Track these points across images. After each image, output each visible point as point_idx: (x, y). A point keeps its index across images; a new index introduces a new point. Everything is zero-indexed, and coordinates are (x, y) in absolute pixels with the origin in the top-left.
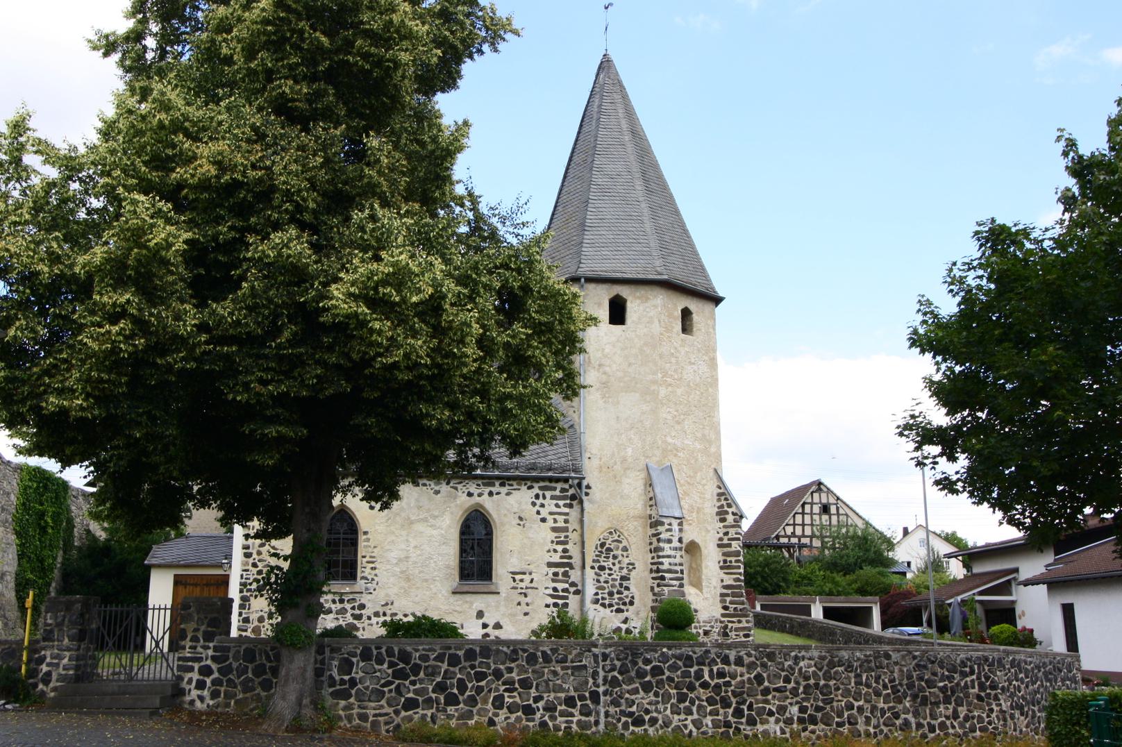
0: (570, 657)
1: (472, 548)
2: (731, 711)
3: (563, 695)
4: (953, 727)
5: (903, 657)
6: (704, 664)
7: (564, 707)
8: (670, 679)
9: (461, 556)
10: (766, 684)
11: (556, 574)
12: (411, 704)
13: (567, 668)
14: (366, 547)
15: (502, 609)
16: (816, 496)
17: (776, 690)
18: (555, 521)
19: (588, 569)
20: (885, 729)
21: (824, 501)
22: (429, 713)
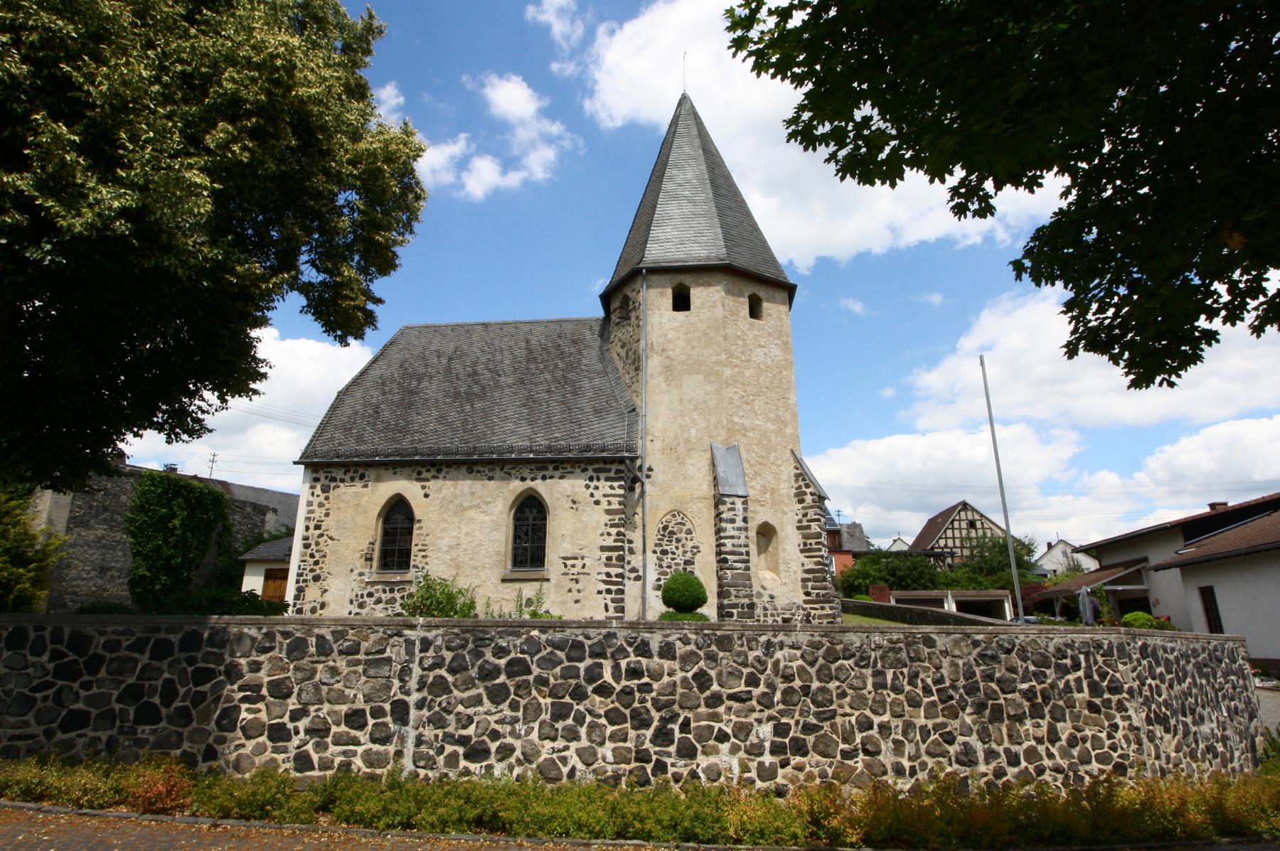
0: (364, 645)
1: (527, 534)
2: (649, 733)
3: (344, 708)
4: (1050, 756)
5: (956, 643)
6: (602, 655)
7: (343, 728)
8: (541, 681)
9: (515, 542)
10: (715, 687)
11: (609, 559)
13: (358, 663)
16: (963, 514)
17: (732, 697)
18: (609, 503)
19: (649, 553)
20: (930, 762)
21: (970, 517)
22: (104, 735)
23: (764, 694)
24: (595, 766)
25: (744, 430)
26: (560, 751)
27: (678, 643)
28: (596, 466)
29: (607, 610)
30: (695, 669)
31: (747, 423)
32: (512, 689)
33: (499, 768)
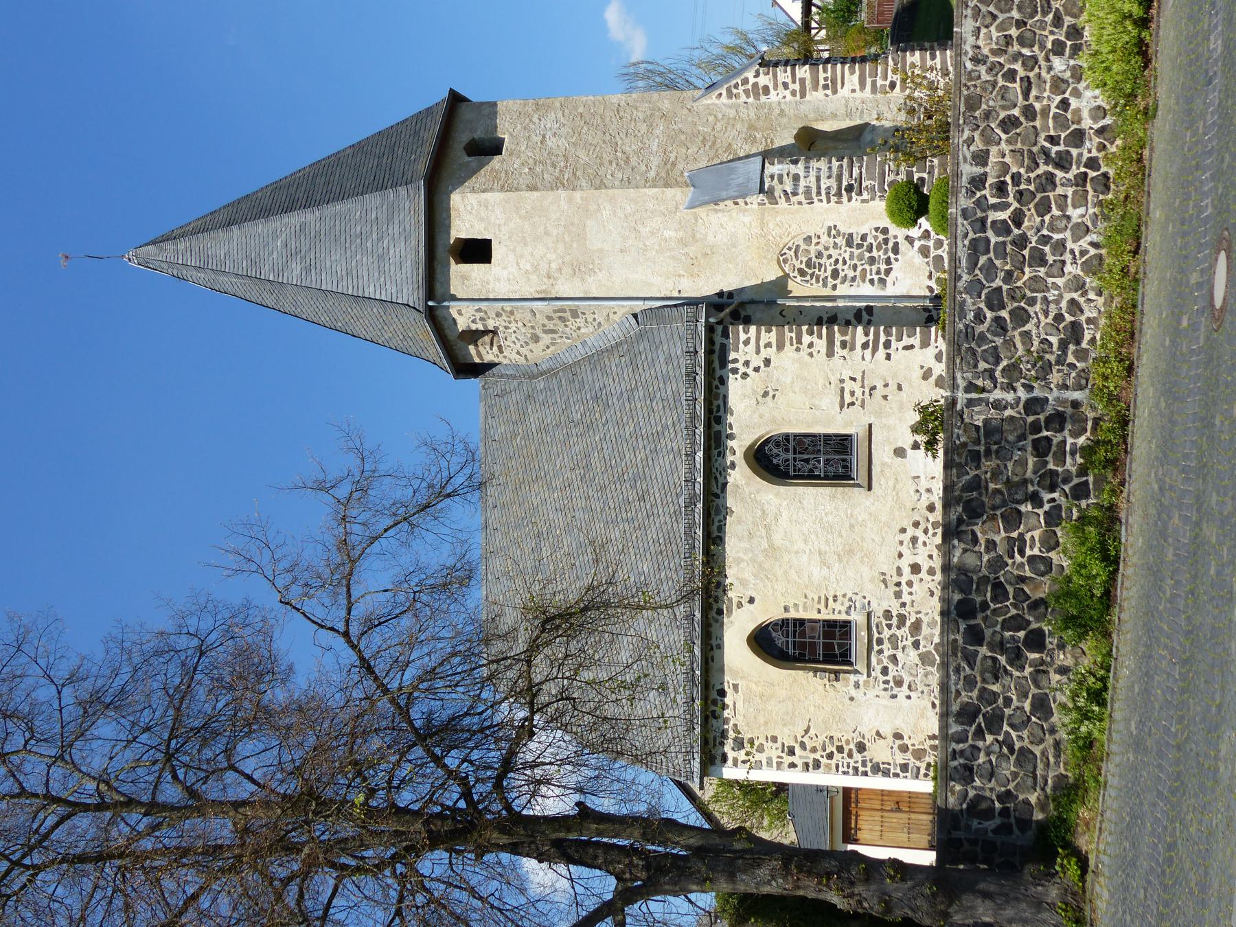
1: (807, 461)
2: (1059, 174)
6: (983, 221)
7: (1050, 458)
10: (1016, 112)
11: (844, 345)
12: (1042, 706)
14: (805, 609)
15: (892, 421)
17: (1026, 95)
18: (768, 345)
19: (837, 293)
23: (1023, 64)
24: (1089, 224)
25: (669, 163)
26: (1074, 257)
27: (972, 148)
28: (716, 364)
29: (912, 347)
30: (998, 131)
31: (655, 161)
32: (1016, 304)
33: (1089, 313)
